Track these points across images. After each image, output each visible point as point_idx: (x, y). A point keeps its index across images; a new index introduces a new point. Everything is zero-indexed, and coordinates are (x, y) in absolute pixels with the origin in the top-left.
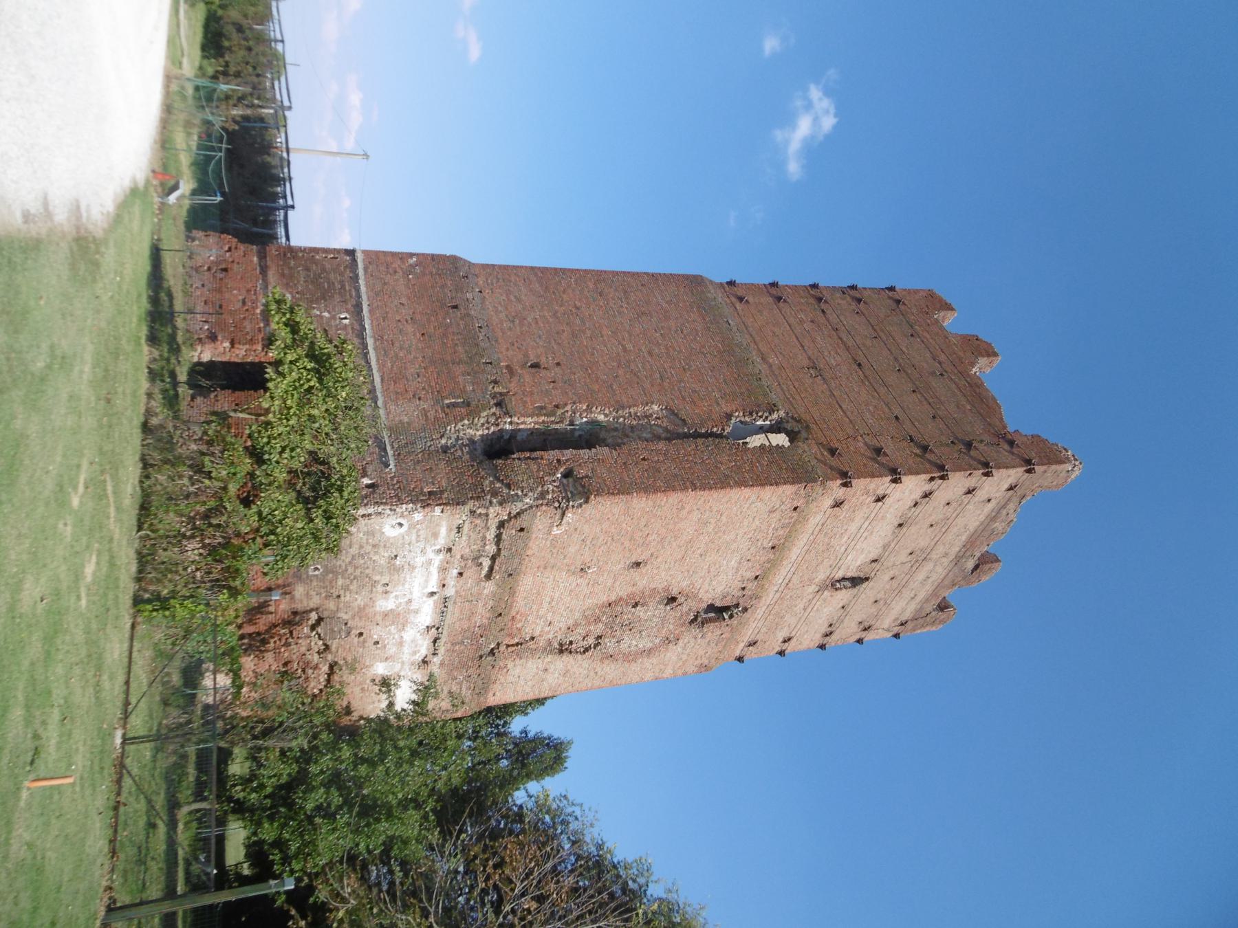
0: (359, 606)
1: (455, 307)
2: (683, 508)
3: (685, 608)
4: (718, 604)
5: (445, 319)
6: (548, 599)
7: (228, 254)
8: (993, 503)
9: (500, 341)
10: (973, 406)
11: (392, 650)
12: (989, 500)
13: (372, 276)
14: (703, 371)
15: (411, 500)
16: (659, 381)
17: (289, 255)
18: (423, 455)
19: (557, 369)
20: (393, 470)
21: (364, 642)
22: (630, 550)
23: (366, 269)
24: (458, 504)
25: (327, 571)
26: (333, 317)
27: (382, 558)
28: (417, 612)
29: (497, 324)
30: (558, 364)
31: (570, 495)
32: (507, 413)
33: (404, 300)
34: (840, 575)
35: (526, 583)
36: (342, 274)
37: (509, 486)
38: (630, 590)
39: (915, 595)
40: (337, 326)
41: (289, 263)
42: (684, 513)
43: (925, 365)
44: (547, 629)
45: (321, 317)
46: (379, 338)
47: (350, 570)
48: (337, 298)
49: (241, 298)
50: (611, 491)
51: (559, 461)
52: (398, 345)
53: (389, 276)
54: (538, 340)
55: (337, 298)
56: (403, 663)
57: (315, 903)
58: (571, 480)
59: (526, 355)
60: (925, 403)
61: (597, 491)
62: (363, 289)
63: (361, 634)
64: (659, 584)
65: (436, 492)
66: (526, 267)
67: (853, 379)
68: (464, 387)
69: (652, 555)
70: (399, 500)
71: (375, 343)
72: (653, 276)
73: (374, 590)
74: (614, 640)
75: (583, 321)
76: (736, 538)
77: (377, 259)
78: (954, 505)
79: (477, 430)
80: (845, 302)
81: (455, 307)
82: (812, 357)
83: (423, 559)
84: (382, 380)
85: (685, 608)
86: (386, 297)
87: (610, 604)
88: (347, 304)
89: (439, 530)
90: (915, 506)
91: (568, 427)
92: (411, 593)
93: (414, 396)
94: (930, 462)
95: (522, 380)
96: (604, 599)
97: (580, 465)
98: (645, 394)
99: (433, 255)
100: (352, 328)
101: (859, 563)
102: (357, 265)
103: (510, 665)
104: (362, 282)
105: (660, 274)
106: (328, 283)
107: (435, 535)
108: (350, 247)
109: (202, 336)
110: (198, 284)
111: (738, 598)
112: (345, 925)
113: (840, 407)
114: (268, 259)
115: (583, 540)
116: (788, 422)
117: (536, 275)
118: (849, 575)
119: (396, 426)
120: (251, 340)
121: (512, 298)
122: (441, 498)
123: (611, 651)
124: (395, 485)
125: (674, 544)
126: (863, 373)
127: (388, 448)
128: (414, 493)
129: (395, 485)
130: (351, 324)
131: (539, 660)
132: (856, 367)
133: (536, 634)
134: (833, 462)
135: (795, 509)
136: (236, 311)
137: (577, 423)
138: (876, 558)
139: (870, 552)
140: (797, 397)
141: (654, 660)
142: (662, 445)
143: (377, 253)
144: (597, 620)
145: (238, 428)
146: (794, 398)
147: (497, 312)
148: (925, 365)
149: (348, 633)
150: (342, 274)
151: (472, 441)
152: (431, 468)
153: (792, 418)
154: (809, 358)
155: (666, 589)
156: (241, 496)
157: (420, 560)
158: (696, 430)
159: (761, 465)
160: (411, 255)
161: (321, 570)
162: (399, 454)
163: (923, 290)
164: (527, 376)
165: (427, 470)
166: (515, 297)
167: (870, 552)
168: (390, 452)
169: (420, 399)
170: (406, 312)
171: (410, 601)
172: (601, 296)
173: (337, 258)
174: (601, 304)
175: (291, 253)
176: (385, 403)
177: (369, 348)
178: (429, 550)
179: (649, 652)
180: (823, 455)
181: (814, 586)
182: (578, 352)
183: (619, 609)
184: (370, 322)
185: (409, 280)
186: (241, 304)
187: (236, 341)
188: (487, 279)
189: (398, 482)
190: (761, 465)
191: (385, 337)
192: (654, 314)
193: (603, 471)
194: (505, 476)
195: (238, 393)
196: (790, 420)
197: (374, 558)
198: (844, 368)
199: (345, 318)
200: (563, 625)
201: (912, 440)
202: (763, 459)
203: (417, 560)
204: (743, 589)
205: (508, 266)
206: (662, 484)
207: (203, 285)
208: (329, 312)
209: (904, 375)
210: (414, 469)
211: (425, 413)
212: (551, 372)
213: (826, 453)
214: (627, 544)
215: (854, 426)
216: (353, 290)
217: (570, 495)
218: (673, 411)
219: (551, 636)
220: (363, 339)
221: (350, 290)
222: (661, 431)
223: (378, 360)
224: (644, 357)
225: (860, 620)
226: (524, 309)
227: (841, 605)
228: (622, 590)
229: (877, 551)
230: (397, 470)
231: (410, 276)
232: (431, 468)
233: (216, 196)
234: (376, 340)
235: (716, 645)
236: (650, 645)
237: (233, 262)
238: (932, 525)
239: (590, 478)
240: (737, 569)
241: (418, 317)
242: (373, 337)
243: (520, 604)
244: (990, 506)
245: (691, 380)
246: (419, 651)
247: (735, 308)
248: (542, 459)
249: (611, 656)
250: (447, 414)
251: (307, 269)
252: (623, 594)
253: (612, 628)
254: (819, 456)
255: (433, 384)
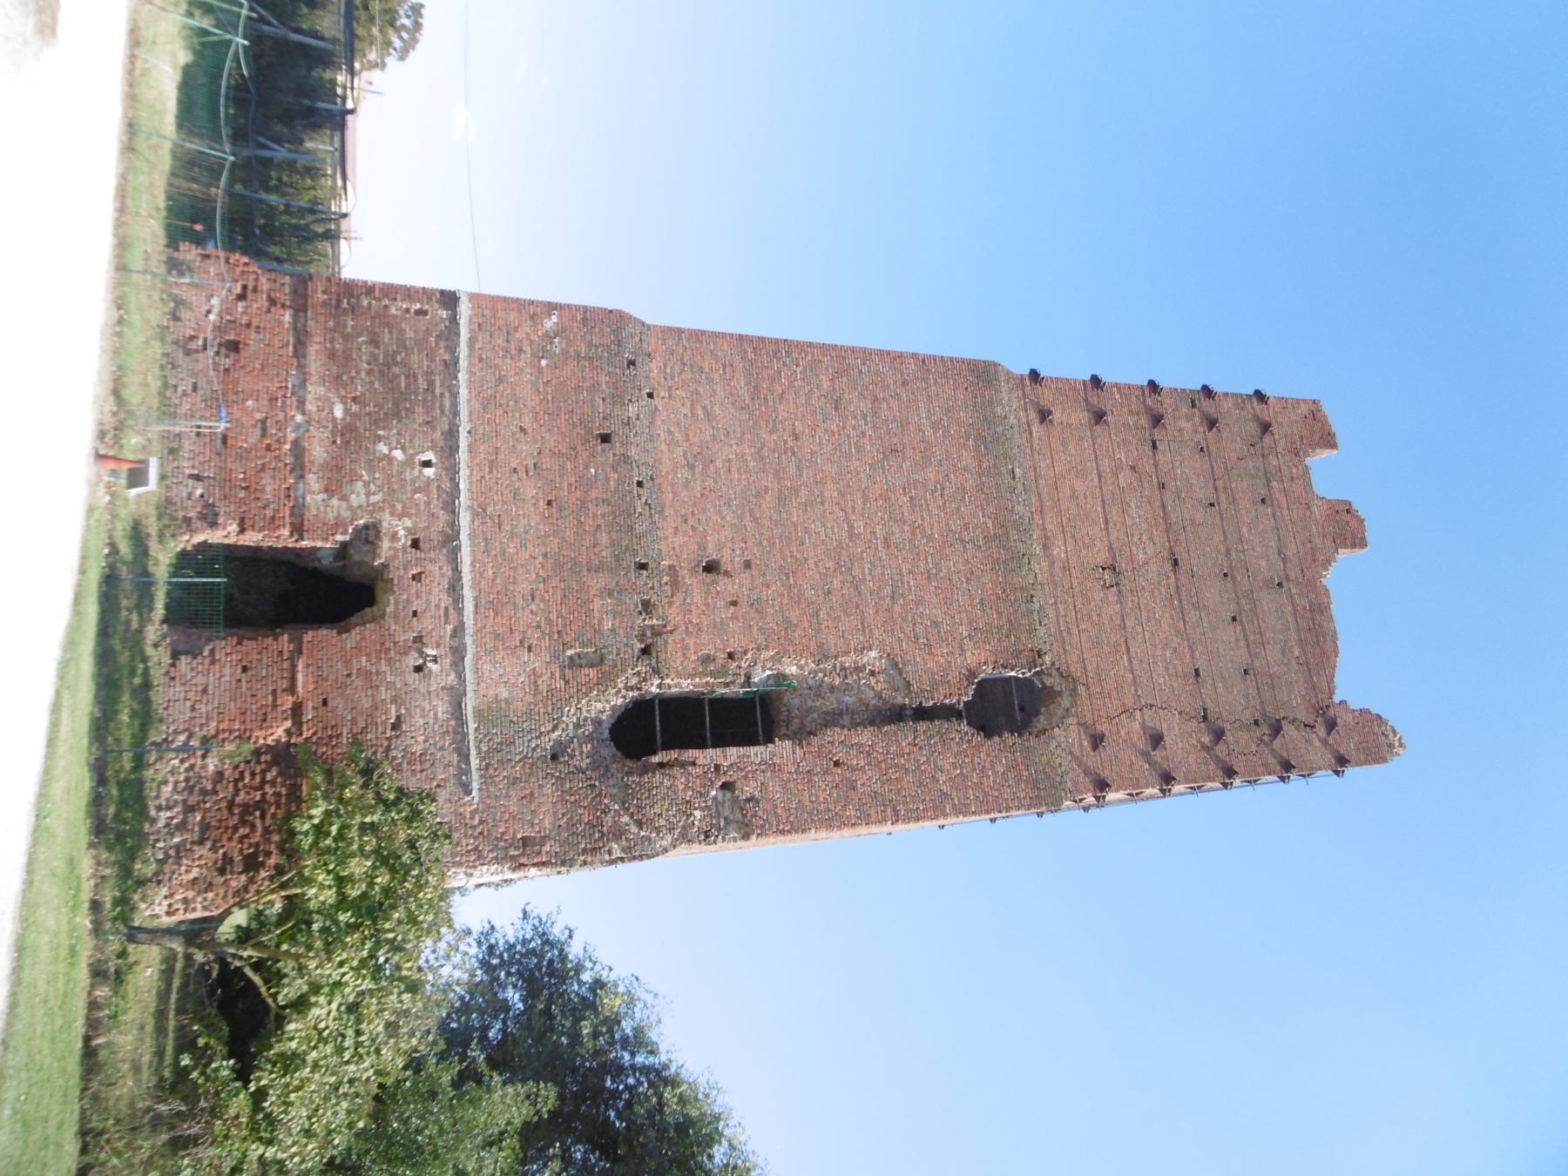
1: (605, 439)
5: (587, 467)
7: (241, 305)
9: (667, 512)
10: (1304, 651)
13: (481, 360)
14: (955, 578)
15: (496, 858)
16: (888, 601)
17: (345, 304)
18: (523, 767)
20: (476, 800)
23: (472, 341)
24: (563, 863)
26: (409, 462)
29: (667, 473)
31: (722, 824)
32: (656, 671)
33: (527, 422)
36: (431, 357)
37: (640, 824)
40: (413, 481)
41: (345, 326)
43: (1263, 563)
45: (389, 459)
46: (479, 513)
48: (420, 415)
49: (258, 416)
50: (781, 827)
51: (717, 767)
52: (508, 528)
53: (508, 361)
54: (725, 511)
57: (341, 69)
58: (729, 795)
59: (702, 546)
60: (1242, 643)
61: (762, 826)
62: (463, 392)
65: (534, 838)
66: (731, 335)
67: (1160, 593)
68: (601, 621)
70: (479, 858)
71: (473, 521)
72: (923, 362)
77: (489, 305)
79: (607, 704)
80: (1190, 425)
81: (605, 439)
82: (1115, 546)
84: (476, 607)
86: (500, 412)
88: (433, 429)
91: (741, 690)
93: (521, 642)
94: (1218, 760)
95: (688, 601)
97: (746, 777)
98: (864, 631)
99: (586, 309)
100: (439, 487)
102: (458, 334)
104: (462, 377)
105: (934, 358)
106: (407, 377)
108: (448, 286)
109: (191, 514)
110: (186, 386)
112: (376, 7)
113: (1128, 649)
114: (309, 313)
116: (1050, 675)
119: (489, 707)
120: (273, 518)
121: (700, 412)
122: (539, 853)
124: (475, 827)
126: (1177, 579)
127: (473, 752)
128: (502, 844)
129: (475, 827)
130: (438, 478)
134: (1092, 760)
136: (249, 451)
137: (756, 680)
140: (1075, 631)
142: (866, 736)
145: (244, 722)
146: (1069, 633)
147: (672, 443)
148: (1263, 563)
150: (431, 357)
151: (597, 722)
152: (532, 794)
153: (1058, 669)
154: (1111, 548)
156: (246, 852)
158: (921, 703)
159: (995, 773)
160: (551, 307)
162: (488, 766)
163: (1305, 401)
164: (694, 582)
165: (525, 797)
166: (704, 408)
168: (474, 762)
172: (836, 409)
173: (425, 313)
174: (834, 428)
175: (351, 294)
176: (477, 658)
177: (461, 537)
180: (1081, 745)
182: (780, 538)
184: (468, 472)
185: (540, 370)
186: (258, 432)
187: (248, 523)
188: (665, 365)
189: (481, 822)
190: (995, 773)
191: (489, 510)
192: (909, 452)
193: (777, 788)
194: (639, 807)
195: (249, 645)
196: (1054, 672)
198: (1153, 568)
201: (1205, 718)
202: (1001, 761)
205: (703, 333)
206: (853, 813)
207: (195, 388)
208: (403, 449)
209: (1229, 586)
210: (508, 796)
212: (734, 584)
213: (1086, 743)
215: (1136, 691)
216: (447, 395)
217: (722, 824)
218: (897, 664)
220: (453, 512)
221: (442, 395)
222: (871, 694)
223: (473, 564)
226: (714, 438)
230: (482, 800)
231: (544, 362)
232: (532, 794)
233: (219, 420)
234: (475, 515)
237: (248, 325)
239: (757, 802)
241: (547, 462)
242: (471, 508)
245: (935, 600)
247: (1031, 433)
248: (694, 764)
250: (567, 682)
251: (374, 342)
254: (1076, 750)
255: (553, 616)
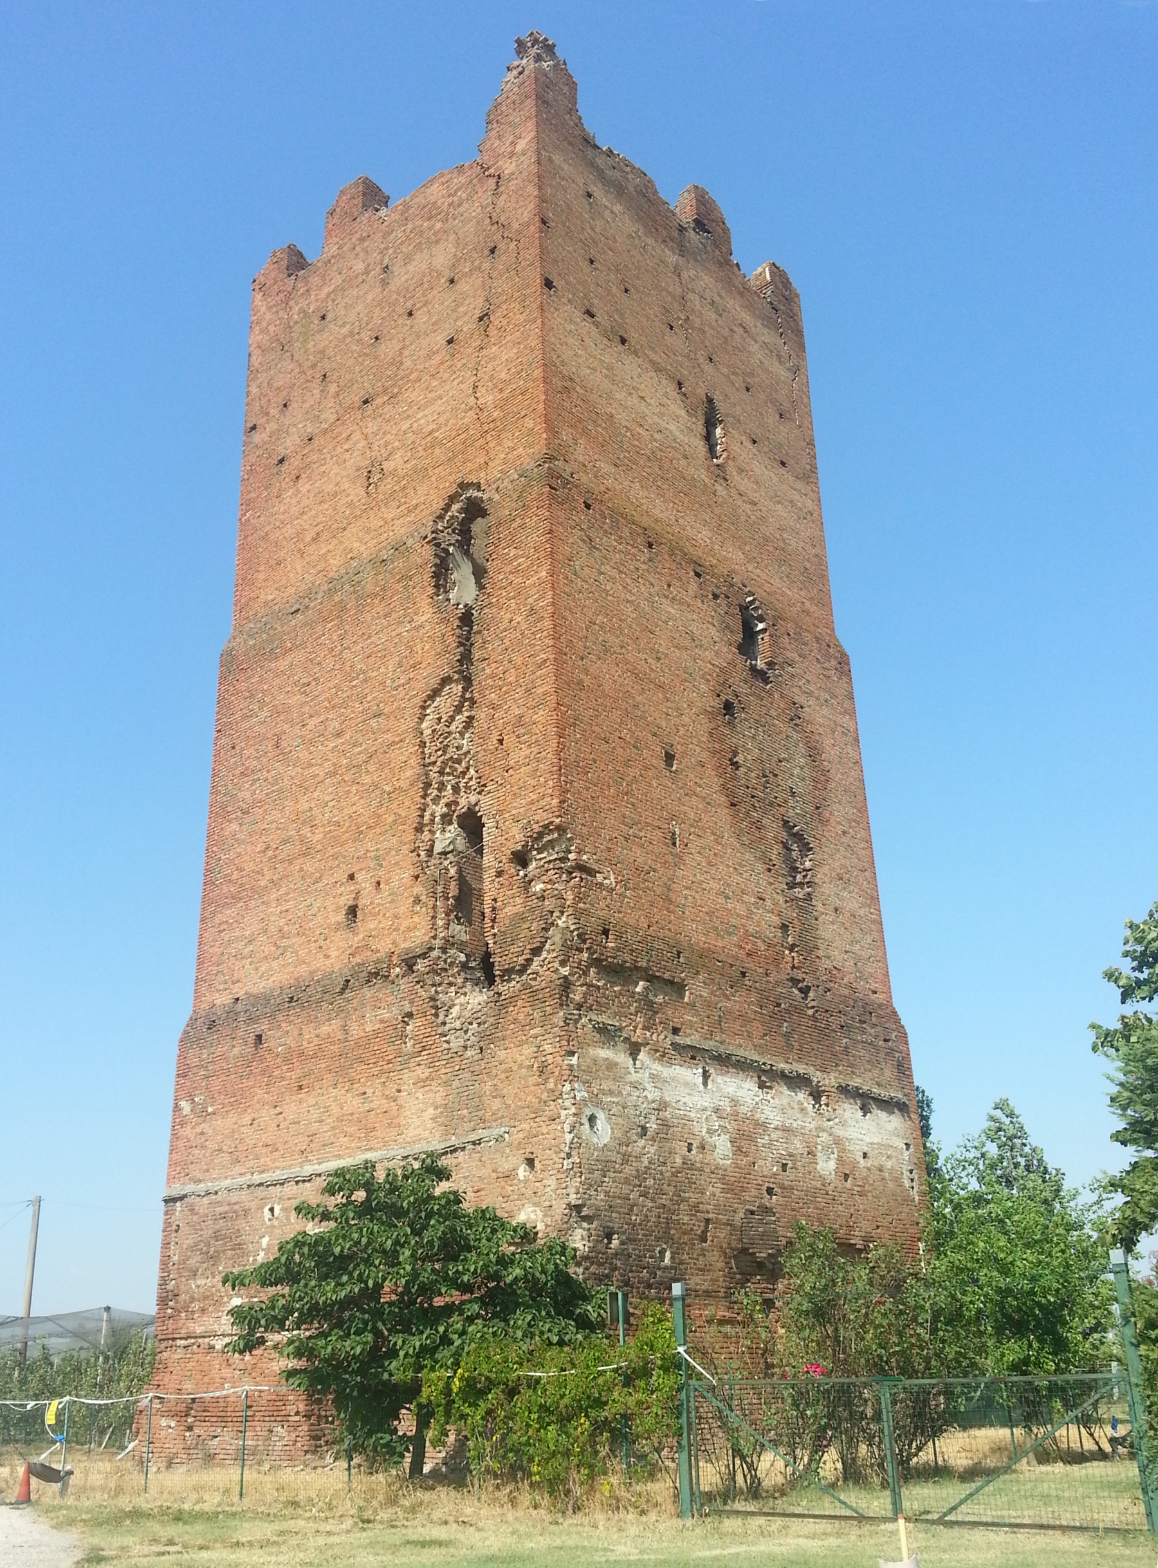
0: (723, 1190)
2: (580, 683)
3: (743, 689)
4: (739, 637)
6: (722, 900)
8: (592, 189)
11: (798, 1146)
12: (590, 196)
19: (359, 877)
21: (783, 1187)
22: (647, 768)
25: (666, 1237)
27: (647, 1150)
28: (735, 1102)
30: (351, 877)
33: (247, 1120)
34: (701, 447)
35: (695, 934)
38: (710, 772)
39: (741, 325)
42: (587, 681)
44: (769, 903)
47: (664, 1200)
55: (241, 1223)
56: (819, 1129)
63: (770, 1191)
64: (702, 727)
69: (655, 735)
73: (698, 1165)
74: (791, 803)
75: (286, 841)
76: (631, 602)
78: (593, 253)
83: (649, 1086)
85: (743, 689)
87: (733, 805)
89: (603, 1058)
90: (593, 316)
92: (705, 1110)
96: (723, 815)
101: (683, 413)
103: (828, 964)
107: (611, 1065)
111: (729, 605)
115: (626, 839)
117: (214, 913)
118: (700, 428)
123: (810, 808)
125: (639, 698)
131: (820, 919)
132: (369, 408)
133: (776, 920)
135: (588, 506)
138: (675, 386)
139: (666, 394)
141: (828, 742)
143: (172, 1164)
144: (758, 826)
149: (767, 1210)
155: (711, 716)
157: (652, 1094)
159: (516, 557)
161: (664, 1246)
167: (666, 394)
169: (399, 1091)
170: (266, 1115)
171: (716, 1110)
178: (634, 1077)
179: (814, 753)
181: (718, 487)
183: (741, 792)
190: (516, 557)
197: (646, 1163)
199: (272, 1210)
200: (764, 878)
203: (650, 1097)
204: (716, 597)
211: (423, 1083)
214: (634, 772)
219: (781, 900)
224: (343, 743)
225: (778, 416)
227: (749, 445)
228: (711, 781)
229: (664, 382)
231: (210, 1110)
235: (805, 644)
236: (802, 748)
238: (626, 291)
240: (681, 603)
243: (727, 945)
244: (598, 191)
246: (800, 1103)
249: (818, 808)
252: (717, 782)
253: (771, 804)
255: (375, 1071)
